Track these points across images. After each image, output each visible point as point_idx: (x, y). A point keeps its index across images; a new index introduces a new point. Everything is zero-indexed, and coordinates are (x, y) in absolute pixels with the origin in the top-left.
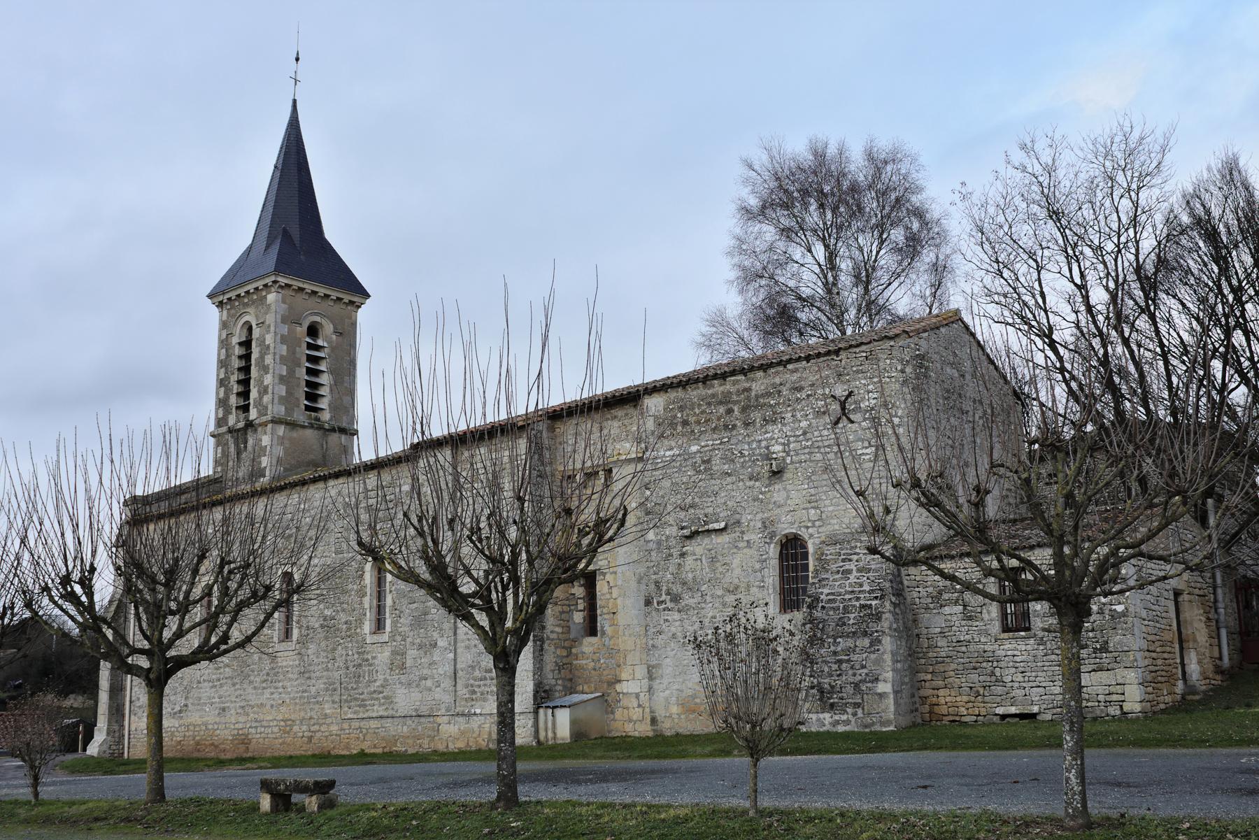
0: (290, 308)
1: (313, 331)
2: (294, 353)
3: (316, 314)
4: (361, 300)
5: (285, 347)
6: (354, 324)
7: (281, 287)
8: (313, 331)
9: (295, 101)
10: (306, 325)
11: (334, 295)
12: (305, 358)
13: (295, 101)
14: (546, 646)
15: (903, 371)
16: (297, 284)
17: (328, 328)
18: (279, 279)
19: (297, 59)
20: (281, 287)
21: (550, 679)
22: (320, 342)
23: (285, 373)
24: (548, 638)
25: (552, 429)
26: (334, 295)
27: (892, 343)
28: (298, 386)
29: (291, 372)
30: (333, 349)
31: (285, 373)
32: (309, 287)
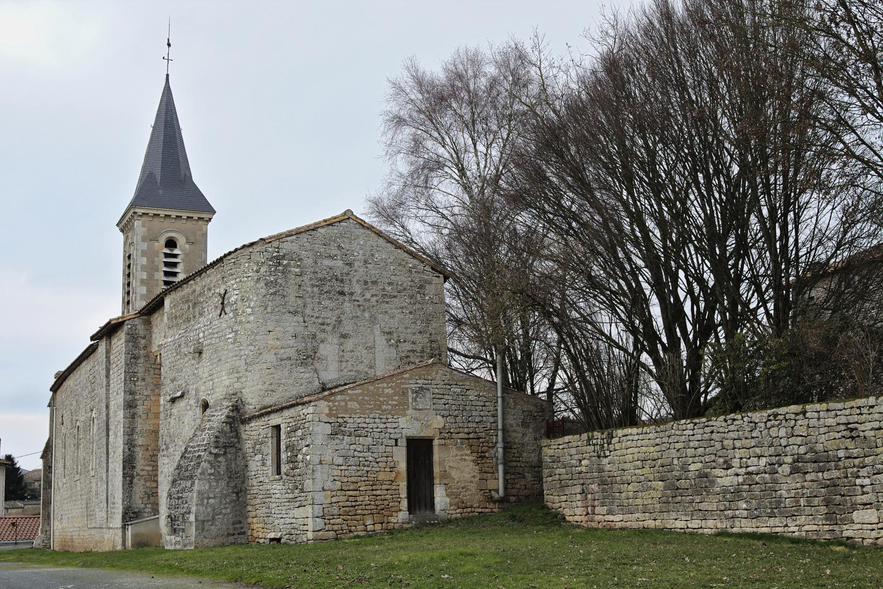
0: (149, 230)
1: (171, 243)
2: (153, 262)
3: (170, 231)
4: (205, 216)
5: (145, 259)
6: (205, 235)
7: (141, 216)
8: (171, 243)
9: (168, 75)
10: (163, 241)
11: (185, 215)
12: (163, 264)
13: (168, 75)
14: (135, 481)
15: (257, 271)
16: (151, 212)
17: (181, 241)
18: (137, 210)
19: (169, 45)
20: (141, 216)
21: (138, 502)
22: (176, 251)
23: (145, 277)
24: (138, 475)
25: (148, 323)
26: (185, 215)
27: (251, 250)
28: (157, 285)
29: (151, 276)
30: (186, 255)
31: (145, 277)
32: (162, 213)
